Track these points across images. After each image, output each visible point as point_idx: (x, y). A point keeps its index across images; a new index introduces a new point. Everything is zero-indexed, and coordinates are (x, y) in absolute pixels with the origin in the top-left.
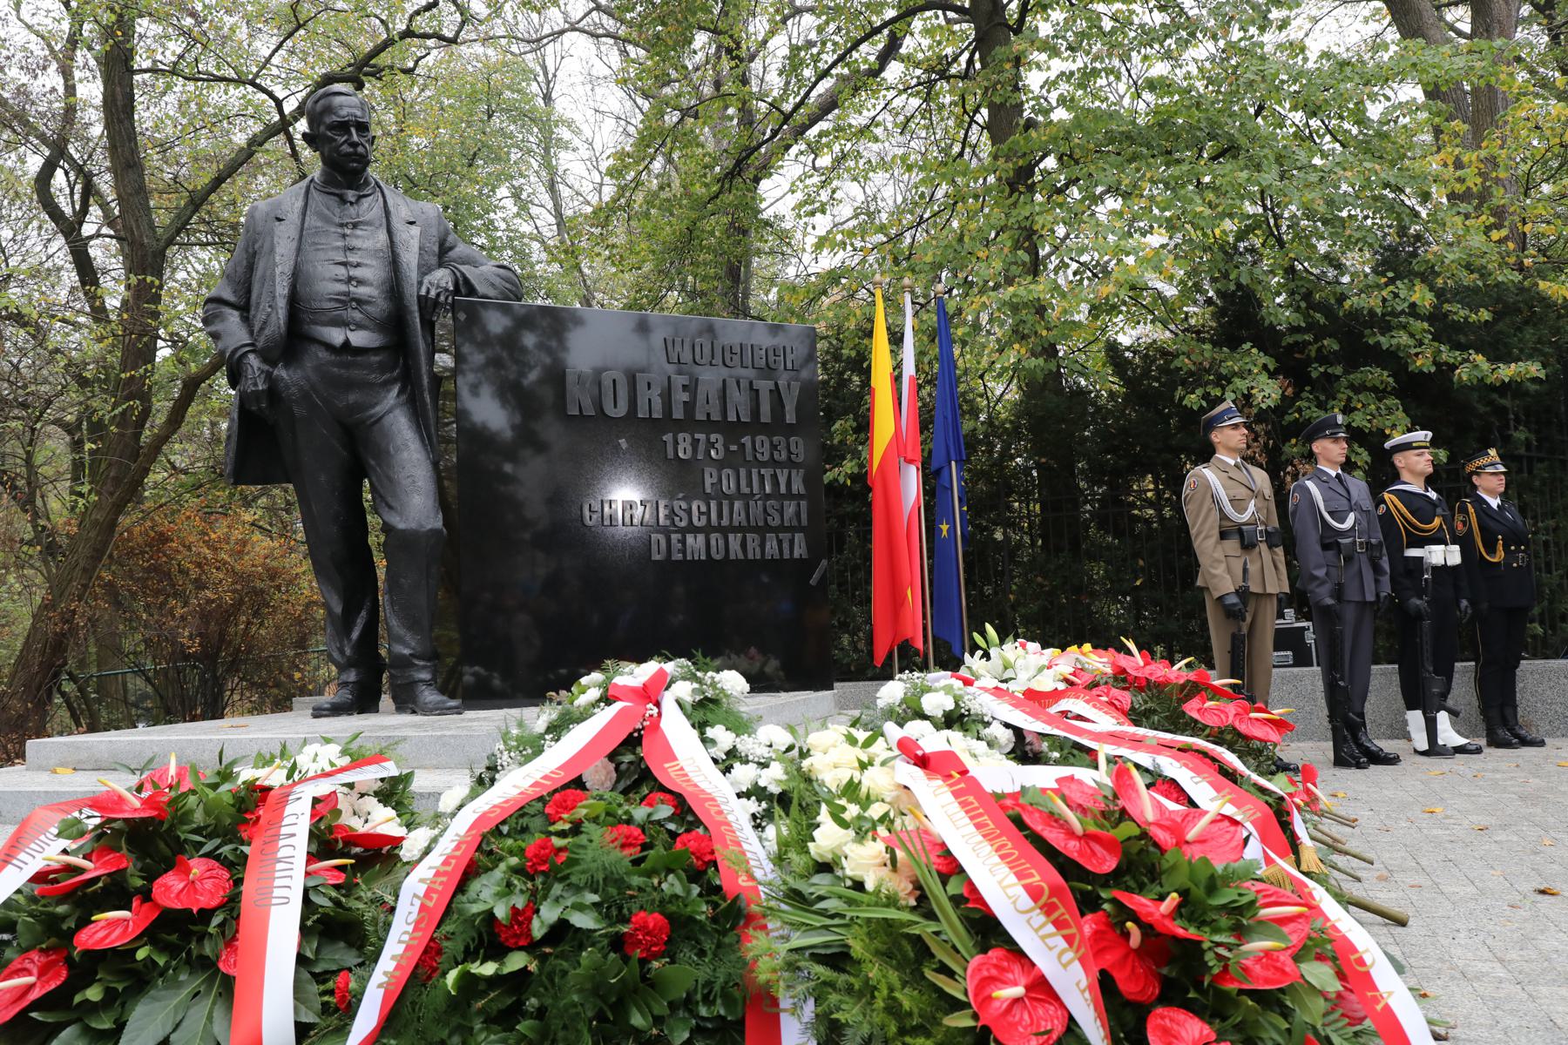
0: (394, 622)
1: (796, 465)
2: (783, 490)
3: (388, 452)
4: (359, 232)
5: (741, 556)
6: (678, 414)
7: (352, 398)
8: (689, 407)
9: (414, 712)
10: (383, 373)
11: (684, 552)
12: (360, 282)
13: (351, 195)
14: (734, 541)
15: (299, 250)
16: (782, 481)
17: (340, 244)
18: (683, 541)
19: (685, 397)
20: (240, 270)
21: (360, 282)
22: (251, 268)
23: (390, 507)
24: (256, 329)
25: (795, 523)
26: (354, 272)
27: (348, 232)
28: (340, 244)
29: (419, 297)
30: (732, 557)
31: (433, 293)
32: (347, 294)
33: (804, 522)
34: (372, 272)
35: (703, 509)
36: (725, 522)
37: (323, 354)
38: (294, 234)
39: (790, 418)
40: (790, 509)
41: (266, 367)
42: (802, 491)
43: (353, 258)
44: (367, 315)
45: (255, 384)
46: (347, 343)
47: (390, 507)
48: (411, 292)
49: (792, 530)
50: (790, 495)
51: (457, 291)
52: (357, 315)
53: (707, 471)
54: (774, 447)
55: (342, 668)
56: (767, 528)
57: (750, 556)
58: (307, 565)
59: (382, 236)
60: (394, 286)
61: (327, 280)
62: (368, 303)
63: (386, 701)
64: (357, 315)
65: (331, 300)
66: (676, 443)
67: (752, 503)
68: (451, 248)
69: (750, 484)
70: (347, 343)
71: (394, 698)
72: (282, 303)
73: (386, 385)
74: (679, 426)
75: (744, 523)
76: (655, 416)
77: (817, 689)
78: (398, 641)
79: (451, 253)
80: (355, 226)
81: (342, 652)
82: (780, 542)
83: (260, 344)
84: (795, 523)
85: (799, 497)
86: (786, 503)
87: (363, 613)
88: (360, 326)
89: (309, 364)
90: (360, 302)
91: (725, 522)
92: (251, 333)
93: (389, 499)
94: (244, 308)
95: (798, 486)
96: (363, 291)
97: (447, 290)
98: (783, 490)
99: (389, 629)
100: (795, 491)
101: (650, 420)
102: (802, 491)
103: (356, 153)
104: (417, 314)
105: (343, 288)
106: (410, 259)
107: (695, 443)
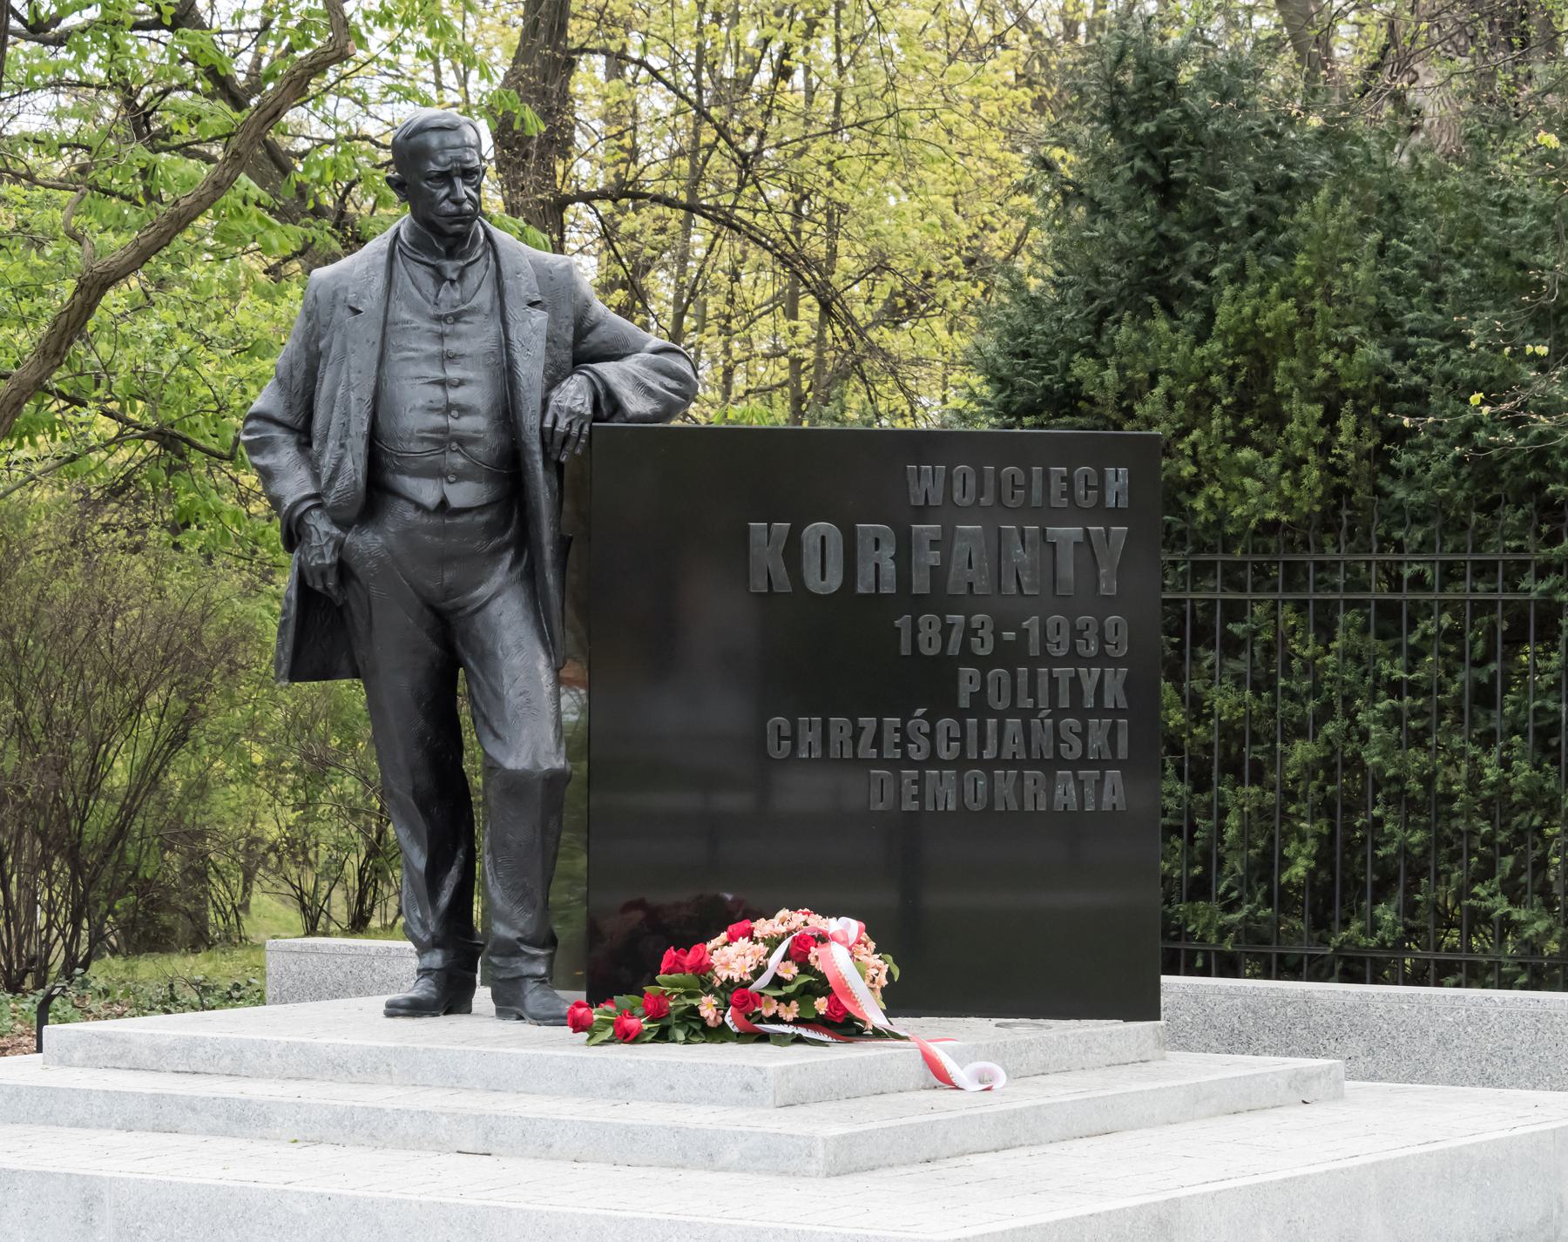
0: (496, 894)
1: (1116, 662)
2: (1089, 703)
3: (494, 654)
4: (461, 327)
5: (1014, 806)
6: (921, 584)
7: (448, 576)
8: (938, 575)
9: (520, 1018)
10: (490, 539)
11: (920, 797)
12: (464, 410)
13: (450, 267)
14: (1005, 781)
15: (382, 360)
16: (1089, 686)
17: (434, 348)
18: (920, 781)
19: (934, 558)
20: (299, 375)
21: (464, 410)
22: (312, 376)
23: (497, 736)
24: (326, 473)
25: (1107, 755)
26: (455, 395)
27: (447, 329)
28: (434, 348)
29: (542, 430)
30: (1000, 807)
31: (562, 424)
32: (445, 430)
33: (1123, 754)
34: (477, 393)
35: (956, 733)
36: (987, 755)
37: (411, 515)
38: (375, 335)
39: (1108, 586)
40: (1098, 730)
41: (335, 531)
42: (1123, 705)
43: (453, 373)
44: (471, 457)
45: (322, 556)
46: (443, 504)
47: (497, 736)
48: (530, 420)
49: (1101, 765)
50: (1099, 710)
51: (597, 414)
52: (459, 461)
53: (966, 671)
54: (1076, 633)
55: (422, 949)
56: (1059, 762)
57: (1029, 807)
58: (278, 535)
59: (494, 328)
60: (507, 412)
61: (414, 406)
62: (474, 441)
63: (483, 996)
64: (459, 461)
65: (423, 439)
66: (915, 630)
67: (1035, 722)
68: (592, 329)
69: (1033, 693)
70: (443, 504)
71: (495, 997)
72: (359, 446)
73: (496, 553)
74: (919, 605)
75: (1022, 756)
76: (885, 590)
77: (1128, 1017)
78: (496, 910)
79: (590, 337)
80: (457, 318)
81: (424, 926)
82: (1080, 784)
83: (330, 501)
84: (1107, 755)
85: (1117, 712)
86: (1093, 721)
87: (454, 871)
88: (461, 476)
89: (391, 526)
90: (462, 441)
91: (988, 754)
92: (316, 477)
93: (495, 724)
94: (303, 434)
95: (1114, 695)
96: (466, 424)
97: (581, 415)
98: (1089, 703)
99: (486, 896)
100: (1109, 704)
101: (877, 597)
102: (1123, 705)
103: (460, 213)
104: (539, 457)
105: (437, 420)
106: (531, 368)
107: (946, 630)
